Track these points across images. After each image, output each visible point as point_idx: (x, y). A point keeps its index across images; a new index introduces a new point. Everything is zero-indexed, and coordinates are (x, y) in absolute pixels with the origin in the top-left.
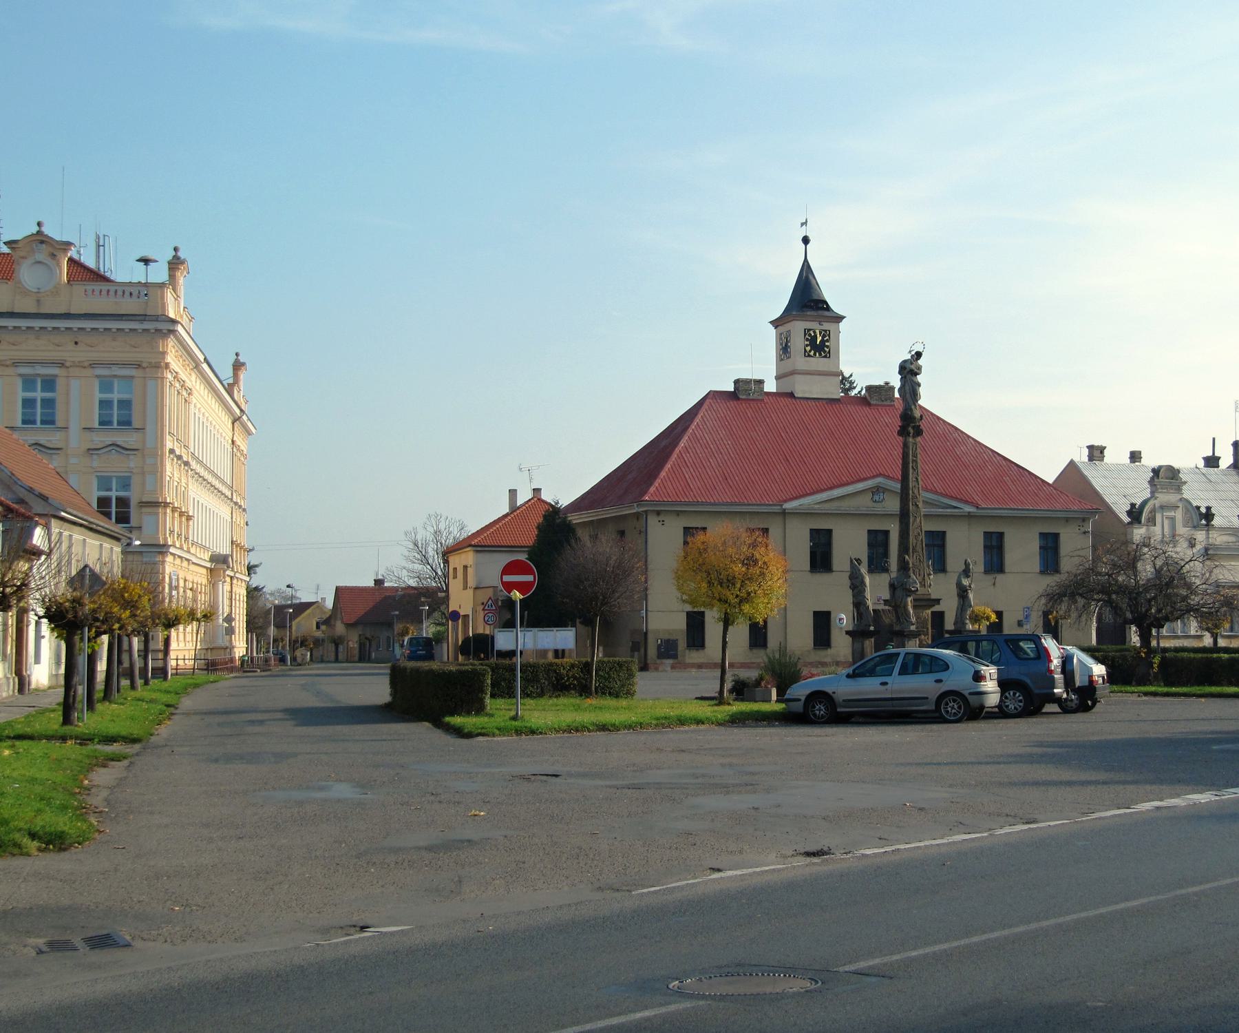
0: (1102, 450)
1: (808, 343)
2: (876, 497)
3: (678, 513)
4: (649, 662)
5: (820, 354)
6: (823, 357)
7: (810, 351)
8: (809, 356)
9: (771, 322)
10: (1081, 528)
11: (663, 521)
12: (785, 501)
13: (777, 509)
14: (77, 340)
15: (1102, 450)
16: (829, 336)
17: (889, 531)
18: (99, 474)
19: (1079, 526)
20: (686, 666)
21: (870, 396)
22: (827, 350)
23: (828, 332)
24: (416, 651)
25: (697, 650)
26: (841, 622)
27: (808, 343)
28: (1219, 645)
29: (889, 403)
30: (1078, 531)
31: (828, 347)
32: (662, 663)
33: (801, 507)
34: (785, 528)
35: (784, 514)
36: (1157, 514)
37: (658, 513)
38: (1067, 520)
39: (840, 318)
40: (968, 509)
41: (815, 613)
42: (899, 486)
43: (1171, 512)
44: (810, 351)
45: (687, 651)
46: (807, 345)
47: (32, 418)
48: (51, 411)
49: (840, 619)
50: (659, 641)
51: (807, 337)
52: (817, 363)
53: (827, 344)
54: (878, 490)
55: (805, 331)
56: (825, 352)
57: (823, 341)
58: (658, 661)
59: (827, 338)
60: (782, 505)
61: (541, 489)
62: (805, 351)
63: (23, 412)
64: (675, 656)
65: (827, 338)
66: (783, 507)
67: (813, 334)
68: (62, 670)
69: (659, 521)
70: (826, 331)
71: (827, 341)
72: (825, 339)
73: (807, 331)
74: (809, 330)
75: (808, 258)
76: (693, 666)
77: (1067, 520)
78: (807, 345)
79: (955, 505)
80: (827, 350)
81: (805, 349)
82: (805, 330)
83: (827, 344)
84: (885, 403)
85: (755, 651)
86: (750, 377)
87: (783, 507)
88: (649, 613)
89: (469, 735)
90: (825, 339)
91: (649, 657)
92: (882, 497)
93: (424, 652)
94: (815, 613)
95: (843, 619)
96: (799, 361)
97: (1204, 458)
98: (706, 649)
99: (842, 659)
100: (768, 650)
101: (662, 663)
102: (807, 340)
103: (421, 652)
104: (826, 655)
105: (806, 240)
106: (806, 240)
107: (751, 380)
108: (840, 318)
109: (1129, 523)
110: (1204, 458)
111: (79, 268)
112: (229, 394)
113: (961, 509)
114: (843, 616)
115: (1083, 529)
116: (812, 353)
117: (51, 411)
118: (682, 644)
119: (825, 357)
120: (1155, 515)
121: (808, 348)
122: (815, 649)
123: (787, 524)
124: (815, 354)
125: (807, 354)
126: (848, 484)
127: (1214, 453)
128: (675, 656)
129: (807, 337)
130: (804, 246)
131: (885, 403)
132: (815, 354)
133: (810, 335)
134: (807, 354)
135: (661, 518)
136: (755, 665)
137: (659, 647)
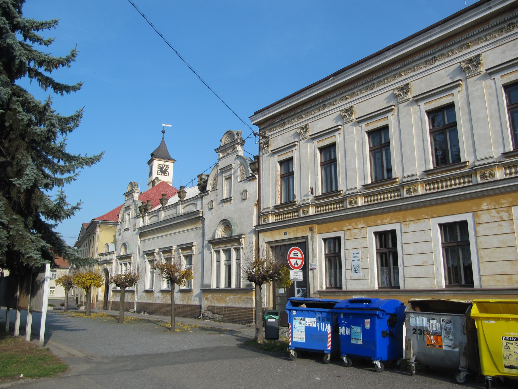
0: (284, 235)
15: (284, 235)
16: (169, 167)
31: (168, 172)
42: (370, 182)
46: (159, 170)
47: (40, 311)
51: (159, 167)
56: (166, 173)
57: (166, 169)
62: (158, 172)
63: (236, 263)
65: (168, 168)
68: (307, 90)
70: (167, 165)
73: (159, 165)
74: (160, 164)
78: (159, 170)
83: (167, 170)
89: (256, 113)
112: (300, 243)
119: (166, 175)
121: (159, 172)
125: (158, 174)
127: (365, 183)
129: (159, 167)
132: (162, 174)
133: (160, 166)
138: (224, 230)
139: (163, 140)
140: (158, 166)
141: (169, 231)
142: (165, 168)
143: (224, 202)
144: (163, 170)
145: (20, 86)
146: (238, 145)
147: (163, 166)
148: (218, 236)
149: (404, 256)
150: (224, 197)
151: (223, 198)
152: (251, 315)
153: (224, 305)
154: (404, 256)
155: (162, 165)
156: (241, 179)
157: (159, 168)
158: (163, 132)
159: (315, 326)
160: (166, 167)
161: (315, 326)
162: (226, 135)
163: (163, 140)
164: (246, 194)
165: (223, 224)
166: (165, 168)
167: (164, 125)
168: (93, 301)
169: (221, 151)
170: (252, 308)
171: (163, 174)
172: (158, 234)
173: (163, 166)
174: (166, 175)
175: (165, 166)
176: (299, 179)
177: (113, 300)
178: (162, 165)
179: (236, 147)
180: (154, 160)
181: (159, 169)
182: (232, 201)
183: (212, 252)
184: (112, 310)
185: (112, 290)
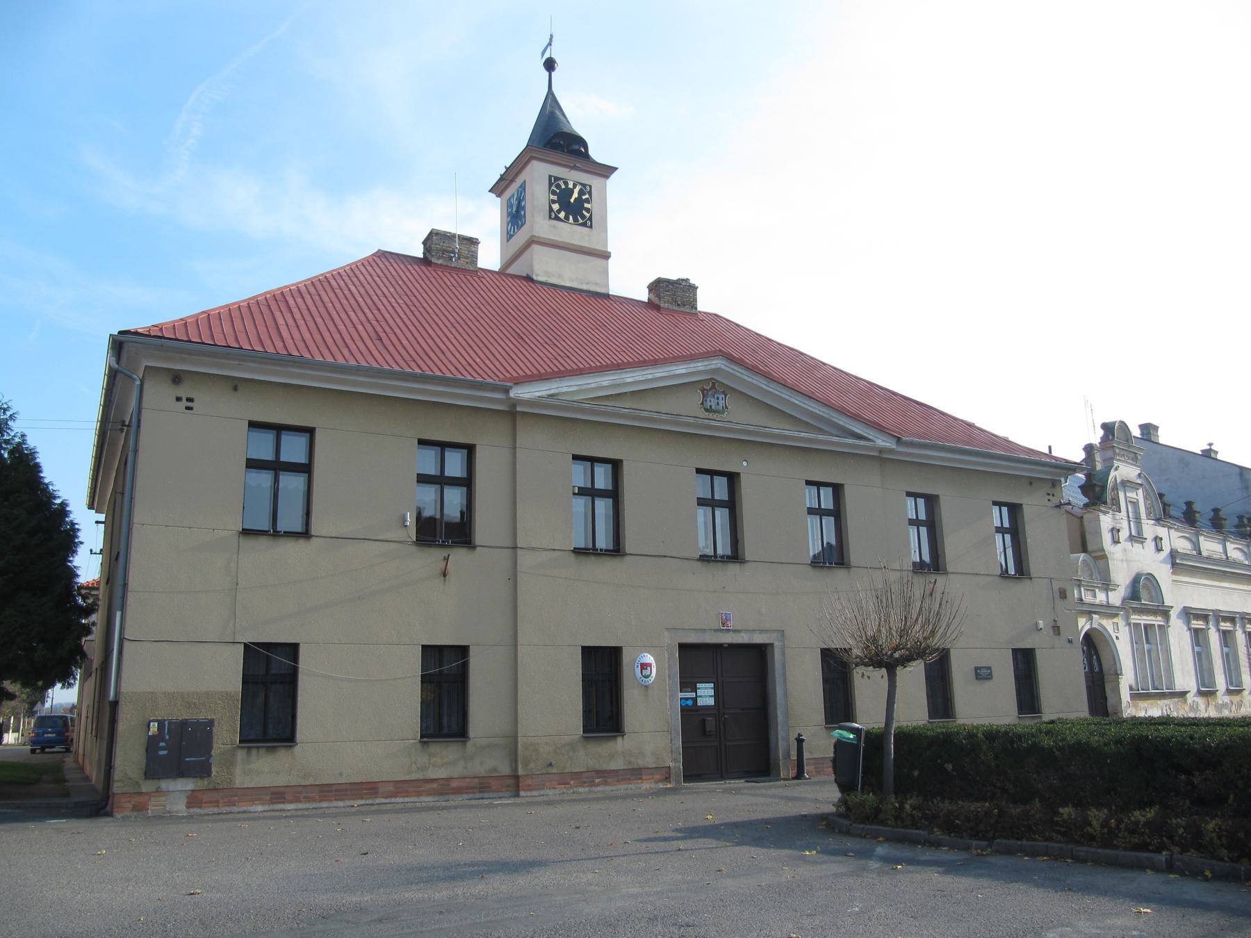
1: (555, 198)
2: (711, 402)
3: (236, 385)
4: (117, 788)
5: (576, 220)
6: (581, 225)
7: (559, 211)
8: (557, 218)
9: (490, 191)
10: (1050, 497)
11: (190, 400)
12: (518, 381)
13: (493, 399)
17: (738, 474)
19: (1049, 494)
20: (234, 795)
21: (658, 296)
22: (587, 215)
23: (588, 188)
24: (43, 734)
25: (271, 750)
26: (646, 672)
28: (699, 704)
29: (688, 310)
30: (1049, 504)
31: (588, 210)
32: (158, 791)
33: (551, 401)
34: (515, 448)
35: (513, 415)
36: (1120, 492)
37: (177, 378)
38: (1031, 482)
39: (606, 171)
40: (882, 442)
41: (584, 648)
43: (1132, 492)
44: (559, 211)
45: (241, 754)
46: (554, 202)
49: (644, 666)
50: (154, 727)
51: (553, 188)
52: (568, 232)
53: (586, 205)
54: (713, 386)
55: (550, 180)
56: (583, 217)
57: (579, 199)
58: (147, 786)
59: (587, 196)
60: (507, 391)
62: (551, 210)
64: (203, 770)
65: (587, 196)
66: (512, 394)
67: (563, 187)
69: (179, 399)
70: (584, 185)
71: (588, 201)
72: (584, 197)
73: (553, 180)
74: (557, 179)
75: (553, 89)
76: (254, 794)
77: (1031, 482)
79: (859, 432)
80: (587, 215)
81: (551, 208)
82: (550, 177)
83: (586, 205)
84: (682, 309)
85: (435, 748)
86: (453, 231)
87: (512, 394)
88: (126, 644)
90: (584, 197)
91: (117, 774)
92: (722, 403)
93: (54, 735)
94: (584, 648)
95: (650, 665)
96: (539, 224)
98: (297, 749)
99: (649, 762)
100: (469, 744)
101: (158, 791)
102: (554, 193)
103: (49, 735)
104: (614, 752)
105: (550, 65)
106: (550, 65)
107: (454, 236)
108: (606, 171)
109: (1086, 506)
113: (872, 441)
114: (649, 658)
115: (1055, 501)
116: (562, 215)
118: (226, 734)
119: (584, 225)
120: (1118, 493)
121: (556, 207)
122: (586, 738)
123: (518, 437)
124: (567, 218)
125: (553, 216)
126: (655, 363)
128: (203, 770)
130: (547, 73)
131: (682, 309)
132: (567, 218)
133: (558, 186)
134: (553, 216)
135: (184, 392)
136: (435, 785)
137: (152, 745)
139: (550, 95)
140: (550, 184)
142: (575, 195)
144: (572, 200)
145: (972, 725)
147: (571, 186)
149: (281, 527)
154: (281, 527)
159: (590, 487)
160: (581, 193)
161: (590, 487)
163: (550, 95)
166: (575, 195)
171: (571, 218)
174: (581, 221)
175: (575, 186)
176: (808, 398)
178: (566, 183)
184: (1154, 625)
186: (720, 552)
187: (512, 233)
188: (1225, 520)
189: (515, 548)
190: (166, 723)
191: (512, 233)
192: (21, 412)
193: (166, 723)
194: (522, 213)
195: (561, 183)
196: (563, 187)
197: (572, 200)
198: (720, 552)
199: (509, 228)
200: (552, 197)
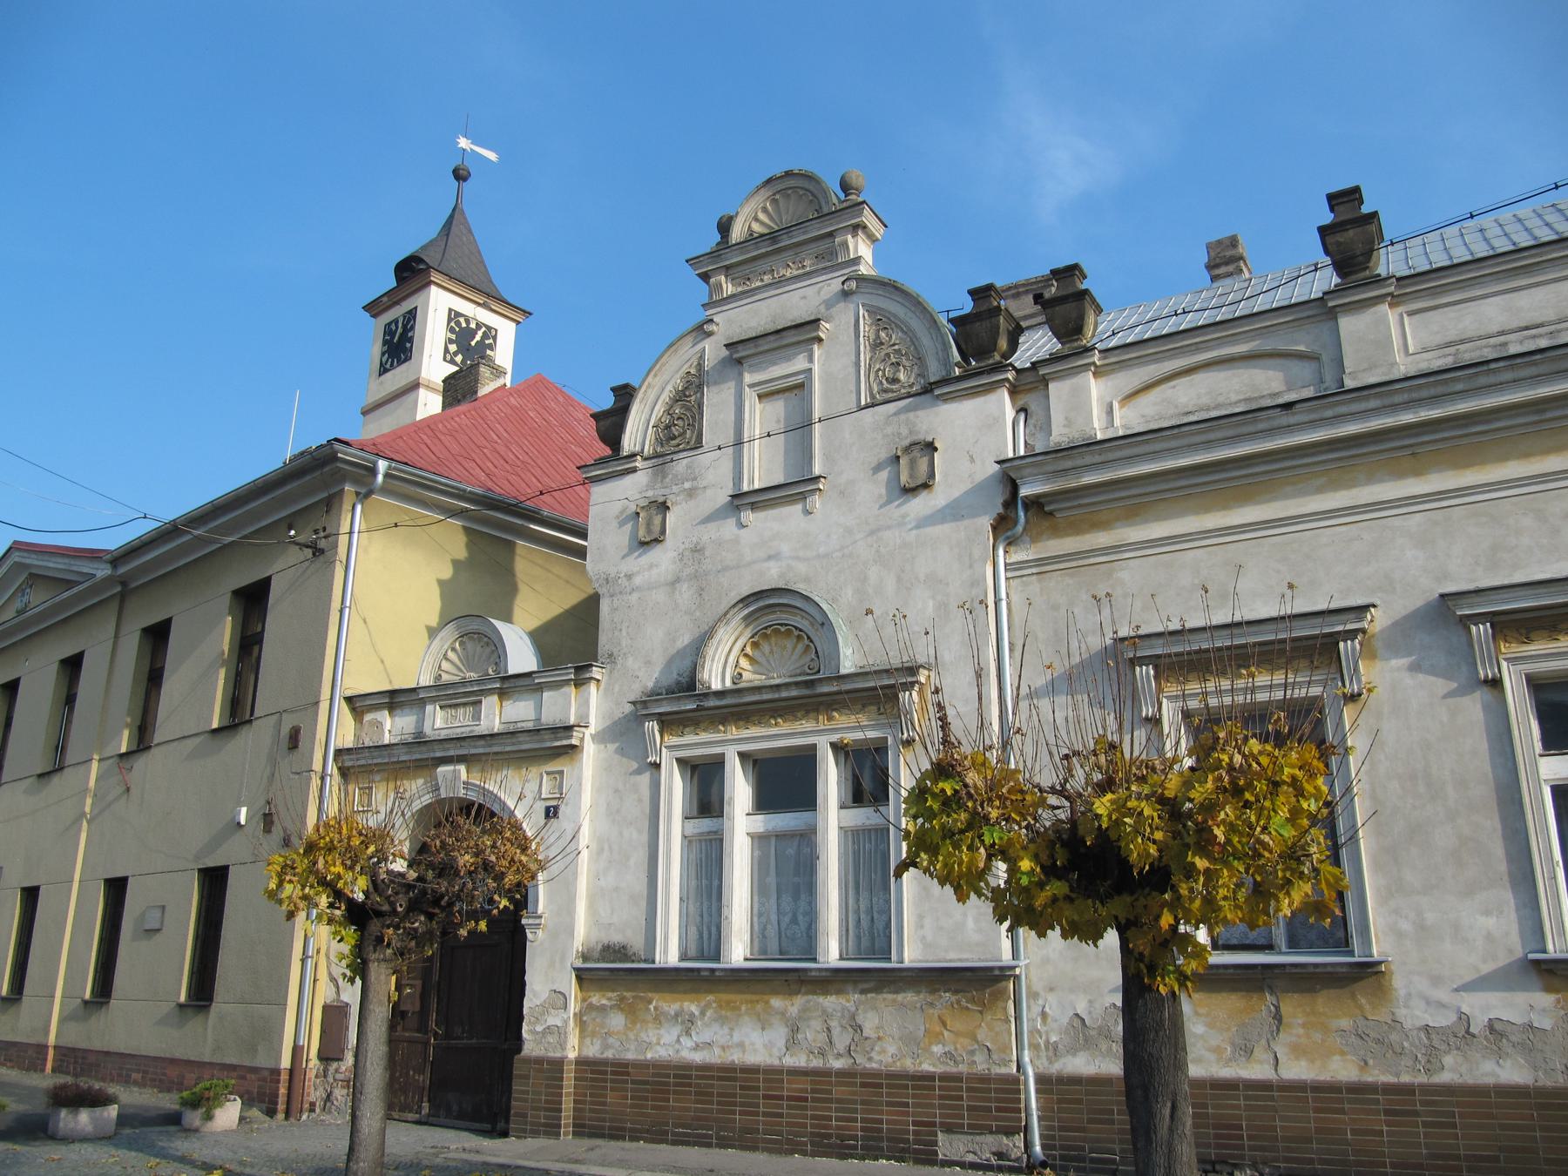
1: (453, 337)
6: (462, 315)
7: (456, 354)
14: (1110, 592)
18: (745, 748)
27: (454, 337)
44: (456, 354)
46: (451, 341)
48: (51, 1053)
51: (453, 324)
59: (491, 341)
61: (1376, 212)
62: (446, 350)
65: (491, 341)
67: (464, 325)
70: (489, 328)
72: (487, 342)
73: (453, 316)
74: (458, 314)
90: (487, 342)
97: (614, 390)
110: (614, 390)
111: (1144, 668)
117: (51, 1053)
121: (453, 348)
125: (448, 358)
129: (453, 324)
133: (458, 324)
138: (748, 650)
140: (450, 320)
141: (1483, 462)
142: (478, 338)
143: (754, 506)
144: (473, 343)
146: (855, 235)
147: (473, 326)
148: (715, 676)
150: (752, 481)
151: (745, 488)
152: (584, 1102)
153: (1342, 1070)
155: (467, 321)
156: (886, 391)
157: (452, 330)
158: (460, 175)
160: (485, 336)
162: (765, 193)
164: (657, 520)
165: (745, 618)
166: (478, 338)
167: (463, 143)
168: (297, 1051)
169: (727, 268)
170: (558, 1065)
172: (1370, 479)
173: (473, 326)
177: (593, 1050)
178: (467, 321)
179: (845, 245)
180: (433, 288)
181: (454, 337)
182: (816, 501)
183: (657, 766)
185: (577, 970)
186: (737, 951)
187: (388, 366)
188: (1450, 695)
189: (1271, 686)
190: (476, 805)
191: (388, 366)
192: (295, 724)
193: (476, 805)
194: (408, 345)
195: (462, 320)
196: (464, 325)
197: (473, 343)
198: (737, 951)
199: (384, 359)
200: (449, 335)
